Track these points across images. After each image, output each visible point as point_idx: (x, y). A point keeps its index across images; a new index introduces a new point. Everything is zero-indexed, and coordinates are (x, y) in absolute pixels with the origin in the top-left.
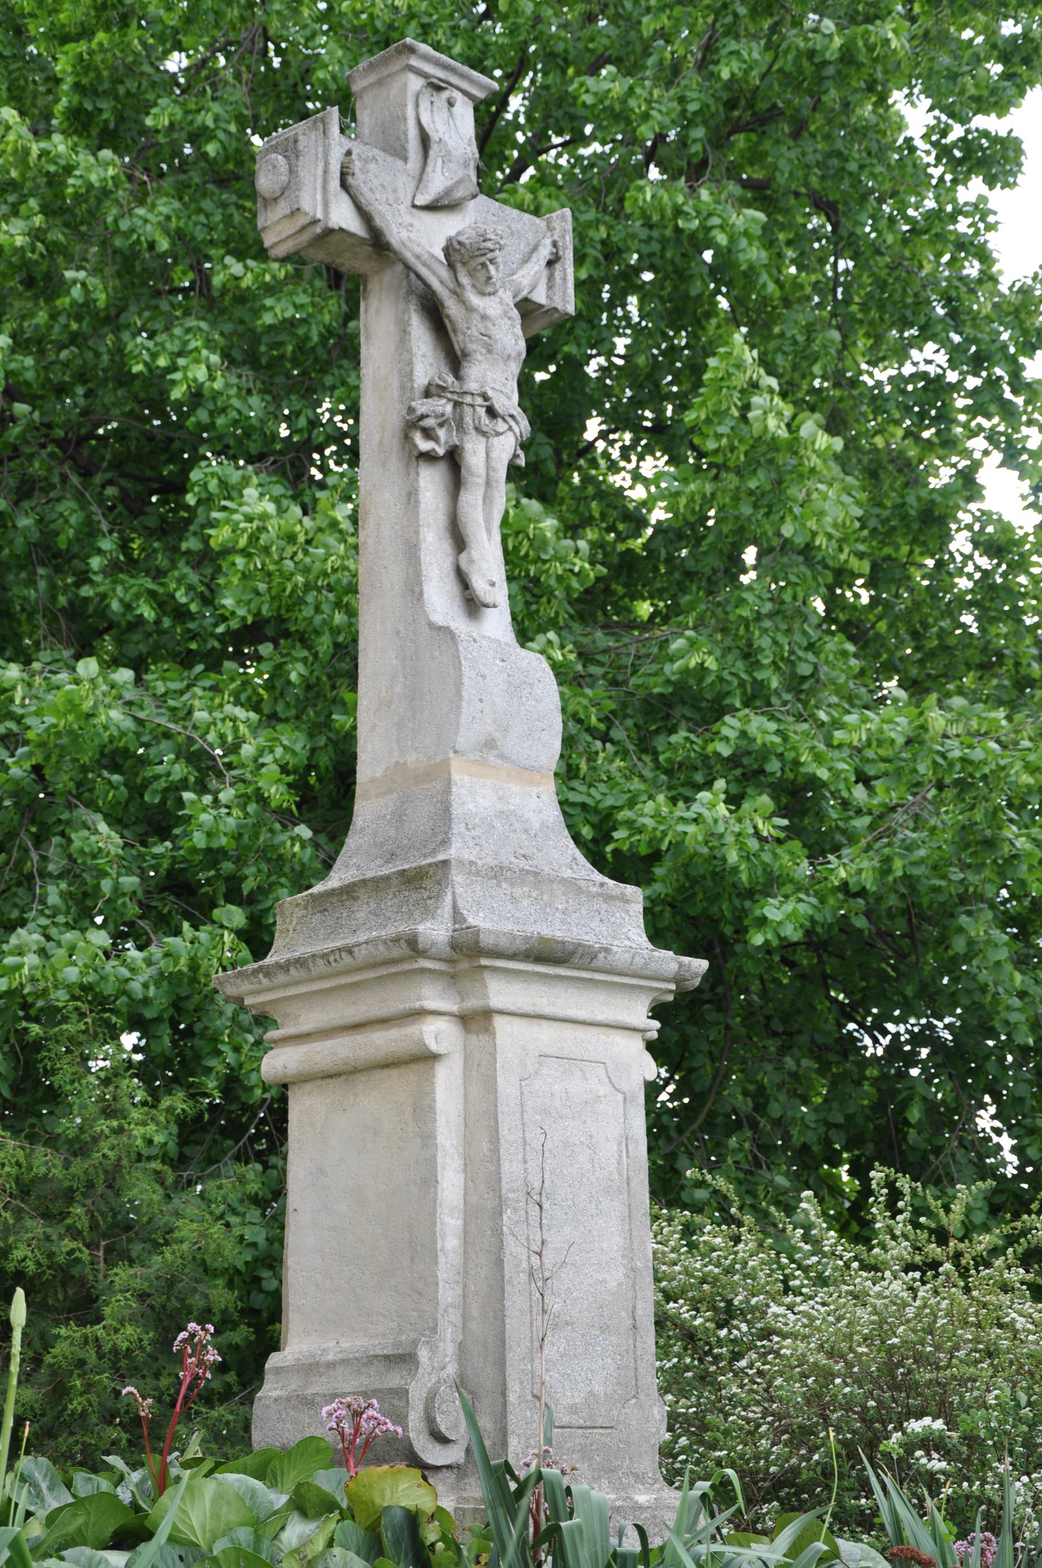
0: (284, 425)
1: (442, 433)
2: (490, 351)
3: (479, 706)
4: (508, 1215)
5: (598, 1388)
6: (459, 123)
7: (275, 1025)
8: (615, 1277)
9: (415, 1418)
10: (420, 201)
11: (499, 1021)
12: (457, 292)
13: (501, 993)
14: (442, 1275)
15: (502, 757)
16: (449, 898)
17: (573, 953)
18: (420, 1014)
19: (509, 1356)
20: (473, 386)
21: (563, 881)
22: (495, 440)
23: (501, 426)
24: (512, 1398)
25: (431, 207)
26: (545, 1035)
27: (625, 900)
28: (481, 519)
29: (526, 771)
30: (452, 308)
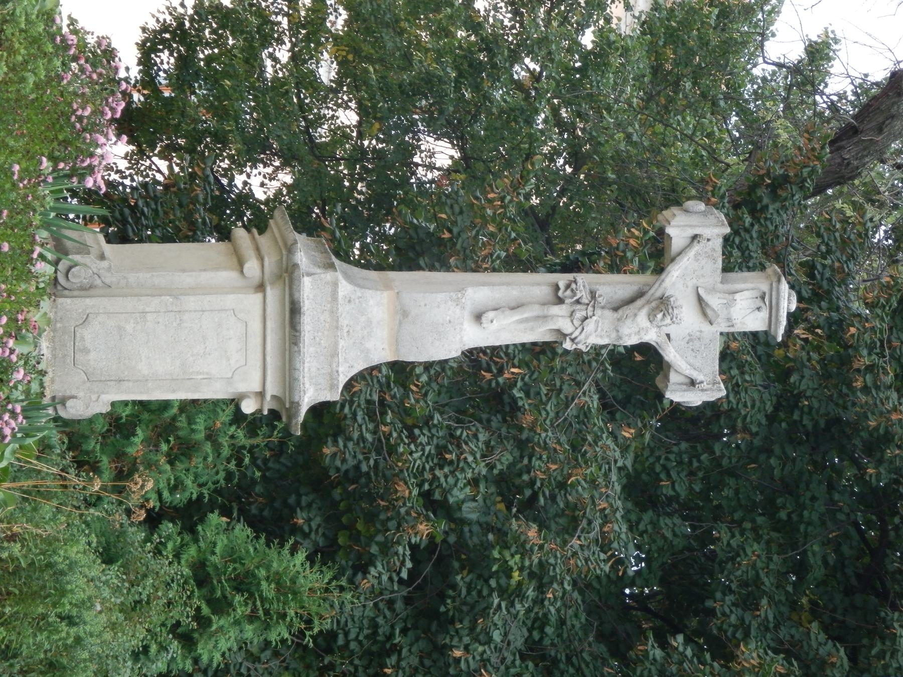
0: (464, 34)
1: (569, 292)
2: (619, 320)
3: (422, 304)
4: (170, 299)
5: (92, 356)
6: (752, 316)
7: (260, 233)
8: (143, 368)
9: (77, 258)
10: (701, 291)
11: (259, 296)
12: (649, 302)
13: (272, 293)
14: (141, 275)
15: (400, 323)
16: (319, 271)
17: (296, 331)
18: (261, 259)
19: (106, 299)
20: (598, 312)
21: (336, 344)
22: (568, 320)
23: (577, 323)
24: (88, 300)
25: (700, 299)
26: (256, 326)
27: (332, 387)
28: (526, 315)
29: (396, 341)
30: (639, 302)
